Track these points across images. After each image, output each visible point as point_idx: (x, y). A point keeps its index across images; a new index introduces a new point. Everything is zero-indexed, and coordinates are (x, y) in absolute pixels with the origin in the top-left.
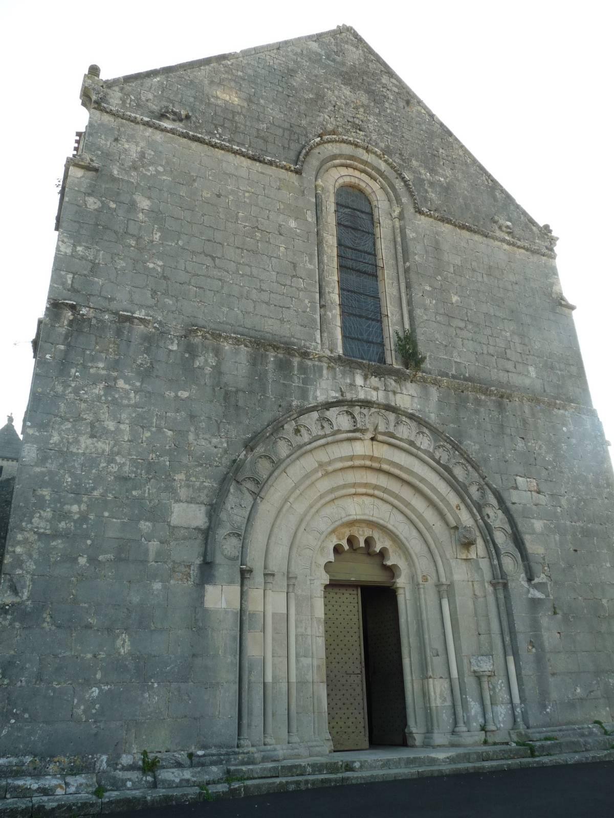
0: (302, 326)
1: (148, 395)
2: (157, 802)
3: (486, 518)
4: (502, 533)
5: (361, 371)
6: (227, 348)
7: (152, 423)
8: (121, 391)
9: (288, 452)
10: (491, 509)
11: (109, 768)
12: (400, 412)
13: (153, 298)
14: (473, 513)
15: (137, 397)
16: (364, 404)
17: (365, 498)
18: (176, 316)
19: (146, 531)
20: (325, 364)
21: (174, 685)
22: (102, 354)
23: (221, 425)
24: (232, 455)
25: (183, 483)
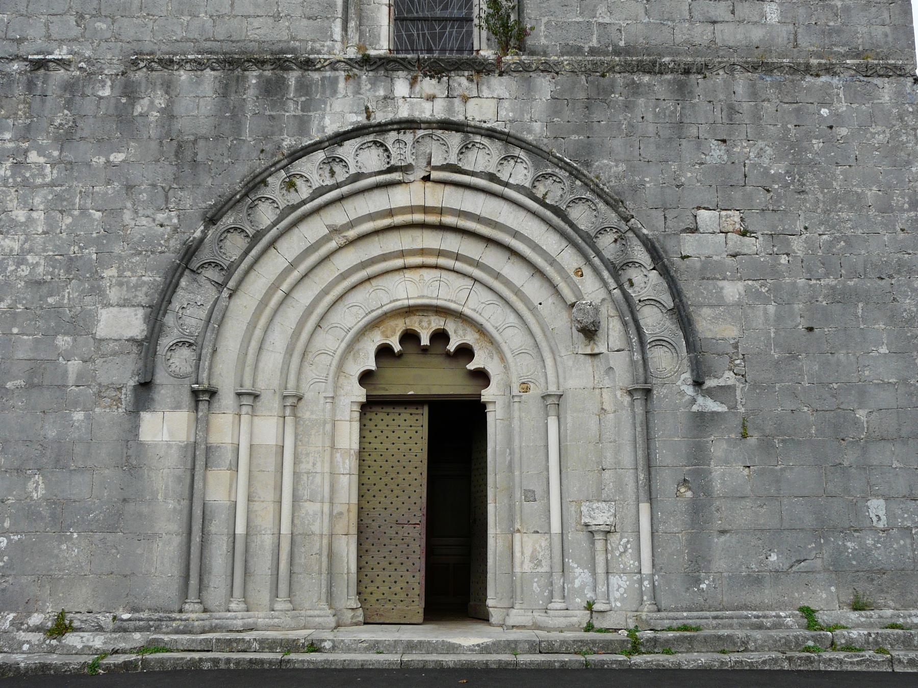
0: (309, 18)
1: (69, 166)
2: (31, 669)
3: (626, 286)
4: (656, 309)
5: (405, 73)
6: (183, 78)
7: (74, 204)
8: (33, 166)
9: (273, 218)
10: (638, 270)
11: (12, 627)
12: (469, 129)
13: (78, 25)
14: (270, 300)
15: (55, 172)
16: (403, 126)
17: (425, 273)
18: (111, 45)
19: (64, 348)
20: (343, 73)
21: (98, 536)
22: (9, 121)
23: (171, 193)
24: (184, 233)
25: (114, 281)
